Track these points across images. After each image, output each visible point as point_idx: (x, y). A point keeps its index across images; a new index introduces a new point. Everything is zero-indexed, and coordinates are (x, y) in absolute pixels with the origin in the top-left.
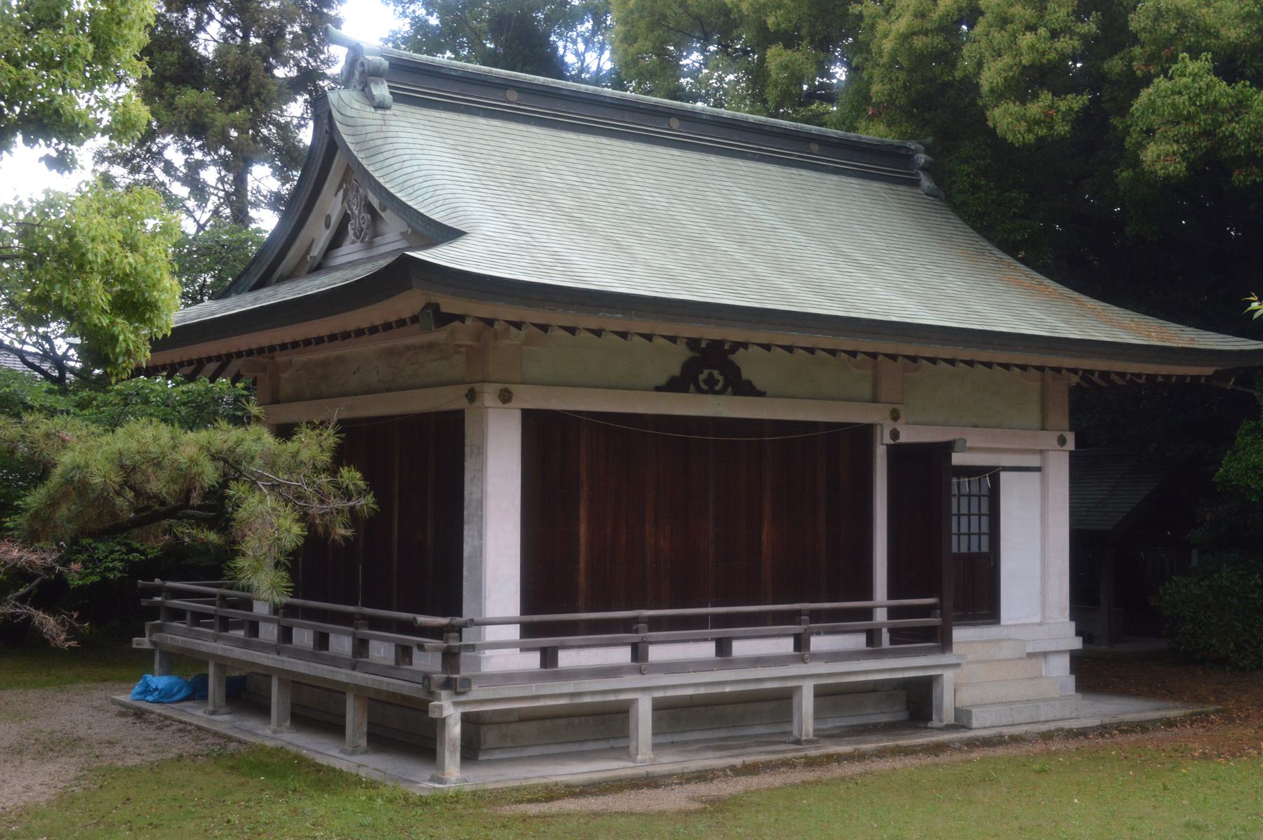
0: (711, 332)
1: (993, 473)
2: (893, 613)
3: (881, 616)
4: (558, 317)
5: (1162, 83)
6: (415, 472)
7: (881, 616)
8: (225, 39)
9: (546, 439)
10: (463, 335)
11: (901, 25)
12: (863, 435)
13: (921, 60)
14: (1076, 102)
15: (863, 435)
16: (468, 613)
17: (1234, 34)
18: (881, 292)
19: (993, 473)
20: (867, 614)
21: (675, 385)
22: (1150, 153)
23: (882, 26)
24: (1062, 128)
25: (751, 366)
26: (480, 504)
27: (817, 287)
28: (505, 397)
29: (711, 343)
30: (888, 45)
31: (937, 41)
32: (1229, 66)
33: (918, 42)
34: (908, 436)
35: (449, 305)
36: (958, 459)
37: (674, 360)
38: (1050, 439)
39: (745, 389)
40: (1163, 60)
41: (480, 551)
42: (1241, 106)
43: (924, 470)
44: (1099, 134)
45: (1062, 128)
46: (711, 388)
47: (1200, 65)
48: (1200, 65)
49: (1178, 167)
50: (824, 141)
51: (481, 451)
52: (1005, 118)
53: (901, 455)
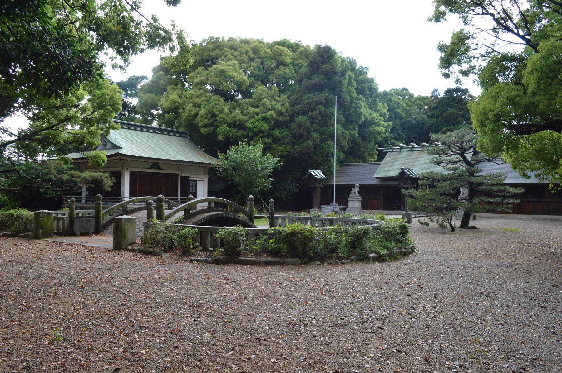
0: (156, 161)
1: (196, 181)
2: (181, 199)
3: (179, 199)
4: (136, 160)
5: (220, 127)
6: (117, 176)
7: (179, 199)
8: (361, 246)
9: (133, 175)
10: (122, 161)
11: (186, 115)
12: (177, 175)
13: (189, 120)
14: (212, 128)
15: (177, 175)
16: (122, 196)
17: (230, 121)
18: (179, 156)
19: (196, 181)
20: (177, 199)
21: (150, 168)
22: (219, 137)
23: (183, 114)
24: (211, 132)
25: (161, 166)
26: (124, 183)
27: (170, 155)
28: (127, 169)
29: (155, 163)
30: (184, 117)
31: (191, 118)
32: (229, 126)
33: (189, 118)
34: (183, 175)
35: (122, 158)
36: (190, 179)
37: (150, 165)
38: (205, 176)
39: (160, 169)
40: (221, 123)
41: (124, 189)
42: (231, 131)
43: (185, 180)
44: (214, 134)
45: (211, 132)
46: (155, 168)
47: (226, 125)
48: (226, 125)
49: (223, 139)
50: (173, 132)
51: (124, 176)
52: (202, 130)
53: (182, 178)
